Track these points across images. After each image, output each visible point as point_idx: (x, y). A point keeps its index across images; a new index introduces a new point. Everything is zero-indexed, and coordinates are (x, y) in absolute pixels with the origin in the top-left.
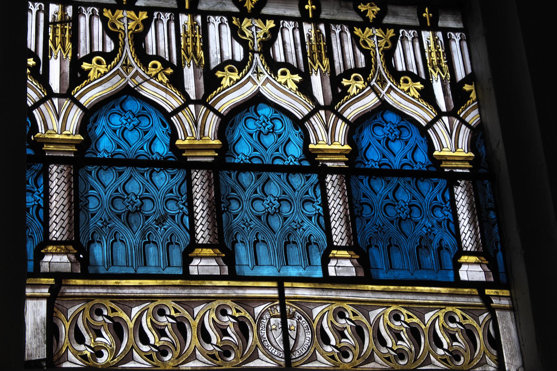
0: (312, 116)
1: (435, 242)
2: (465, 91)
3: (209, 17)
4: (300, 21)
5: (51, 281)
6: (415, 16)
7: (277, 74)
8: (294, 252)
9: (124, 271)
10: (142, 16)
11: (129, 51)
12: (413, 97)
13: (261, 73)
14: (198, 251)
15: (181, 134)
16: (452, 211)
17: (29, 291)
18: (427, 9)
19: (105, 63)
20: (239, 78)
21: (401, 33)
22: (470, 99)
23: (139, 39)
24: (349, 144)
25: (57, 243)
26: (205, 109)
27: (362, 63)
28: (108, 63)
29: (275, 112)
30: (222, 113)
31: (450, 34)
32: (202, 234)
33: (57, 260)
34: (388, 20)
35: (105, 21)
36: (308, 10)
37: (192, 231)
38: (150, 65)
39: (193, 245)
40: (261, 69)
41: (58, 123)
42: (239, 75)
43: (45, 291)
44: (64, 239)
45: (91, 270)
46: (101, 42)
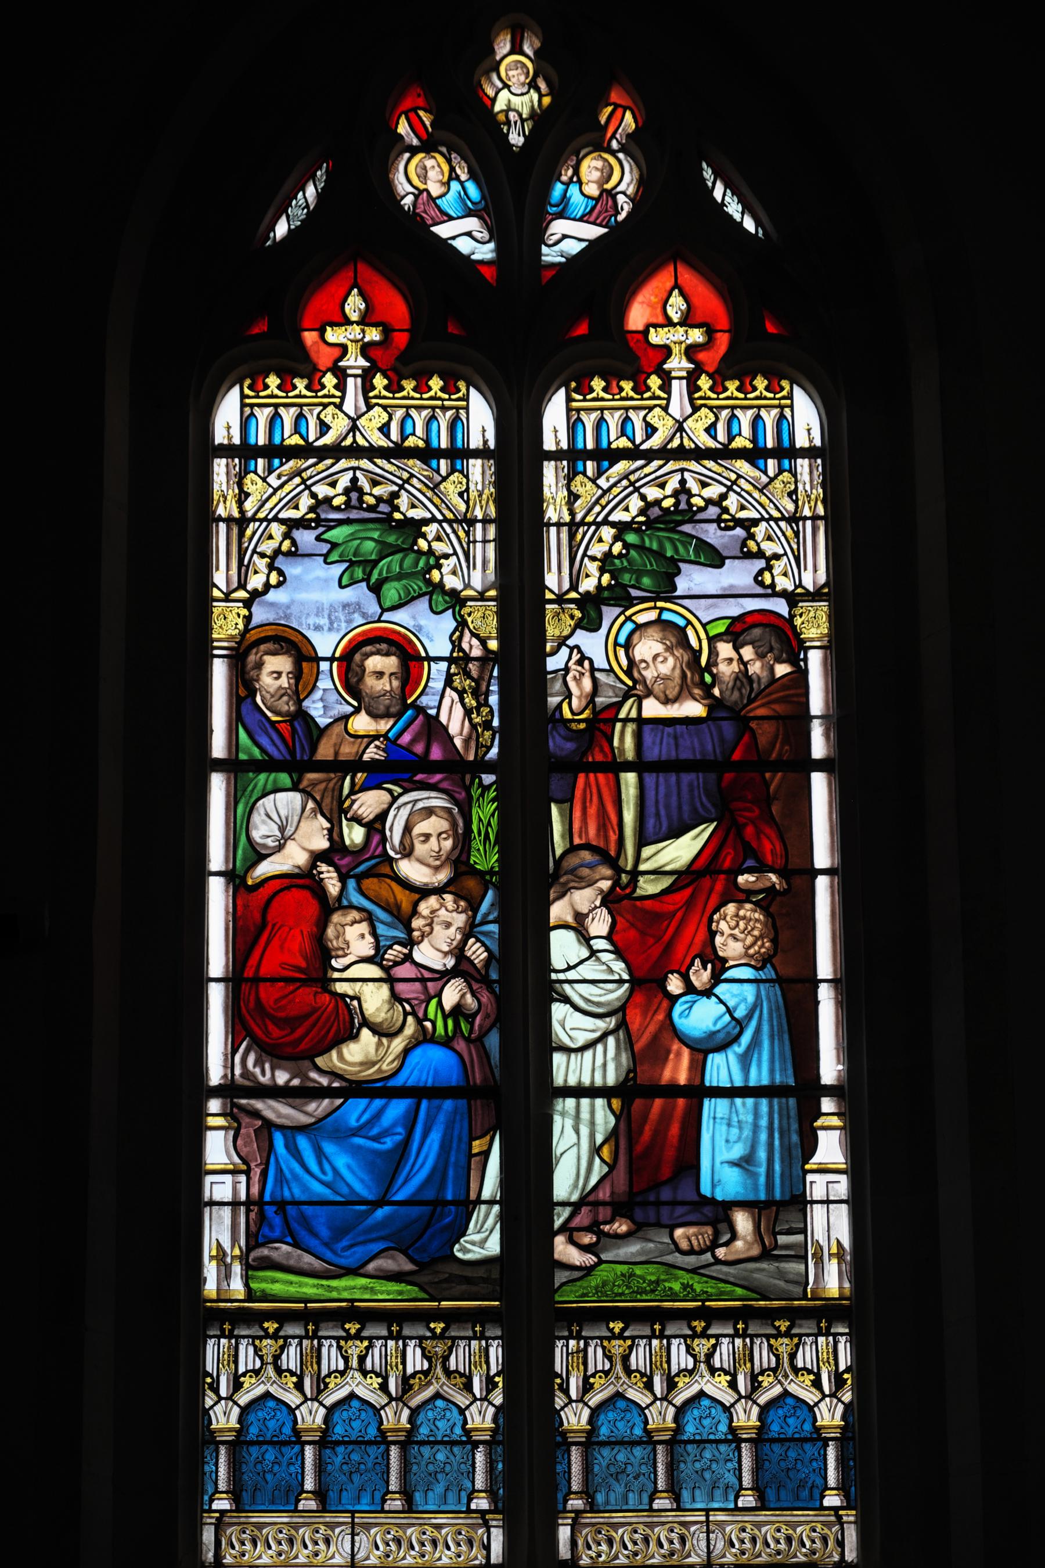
5: (573, 1515)
9: (614, 1508)
11: (619, 1368)
15: (385, 1423)
17: (560, 1521)
25: (575, 1493)
27: (773, 1364)
32: (832, 1481)
33: (576, 1503)
39: (656, 1491)
40: (705, 1373)
41: (224, 1418)
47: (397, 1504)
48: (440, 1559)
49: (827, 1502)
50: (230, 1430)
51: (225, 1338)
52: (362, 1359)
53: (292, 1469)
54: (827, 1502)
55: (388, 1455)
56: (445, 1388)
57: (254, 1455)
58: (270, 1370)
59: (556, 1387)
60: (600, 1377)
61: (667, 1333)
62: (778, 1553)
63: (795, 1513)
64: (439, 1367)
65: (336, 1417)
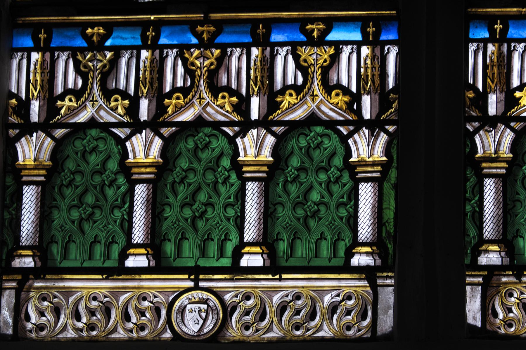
0: (54, 136)
1: (329, 237)
2: (515, 97)
3: (342, 47)
4: (247, 47)
6: (138, 36)
7: (110, 100)
8: (213, 248)
10: (329, 51)
12: (227, 111)
13: (317, 96)
14: (247, 249)
16: (129, 211)
18: (261, 26)
19: (182, 98)
20: (296, 101)
21: (165, 53)
22: (280, 109)
23: (212, 75)
24: (386, 156)
25: (138, 246)
26: (265, 131)
28: (298, 94)
29: (101, 132)
30: (56, 136)
31: (277, 50)
32: (138, 235)
33: (492, 257)
34: (331, 37)
35: (297, 58)
36: (148, 36)
37: (129, 233)
38: (220, 95)
39: (242, 244)
40: (204, 95)
42: (297, 98)
43: (480, 280)
44: (368, 241)
45: (164, 264)
46: (293, 76)
47: (257, 261)
48: (64, 329)
49: (356, 261)
50: (374, 164)
51: (257, 46)
52: (326, 71)
53: (117, 214)
54: (356, 261)
55: (244, 195)
56: (102, 113)
57: (293, 195)
58: (317, 88)
59: (11, 110)
60: (70, 100)
61: (163, 41)
62: (142, 328)
63: (144, 277)
64: (96, 87)
65: (69, 150)
